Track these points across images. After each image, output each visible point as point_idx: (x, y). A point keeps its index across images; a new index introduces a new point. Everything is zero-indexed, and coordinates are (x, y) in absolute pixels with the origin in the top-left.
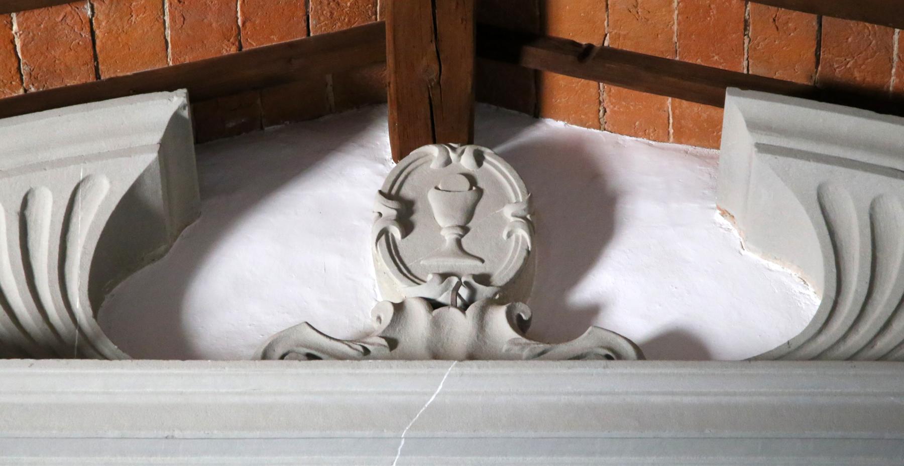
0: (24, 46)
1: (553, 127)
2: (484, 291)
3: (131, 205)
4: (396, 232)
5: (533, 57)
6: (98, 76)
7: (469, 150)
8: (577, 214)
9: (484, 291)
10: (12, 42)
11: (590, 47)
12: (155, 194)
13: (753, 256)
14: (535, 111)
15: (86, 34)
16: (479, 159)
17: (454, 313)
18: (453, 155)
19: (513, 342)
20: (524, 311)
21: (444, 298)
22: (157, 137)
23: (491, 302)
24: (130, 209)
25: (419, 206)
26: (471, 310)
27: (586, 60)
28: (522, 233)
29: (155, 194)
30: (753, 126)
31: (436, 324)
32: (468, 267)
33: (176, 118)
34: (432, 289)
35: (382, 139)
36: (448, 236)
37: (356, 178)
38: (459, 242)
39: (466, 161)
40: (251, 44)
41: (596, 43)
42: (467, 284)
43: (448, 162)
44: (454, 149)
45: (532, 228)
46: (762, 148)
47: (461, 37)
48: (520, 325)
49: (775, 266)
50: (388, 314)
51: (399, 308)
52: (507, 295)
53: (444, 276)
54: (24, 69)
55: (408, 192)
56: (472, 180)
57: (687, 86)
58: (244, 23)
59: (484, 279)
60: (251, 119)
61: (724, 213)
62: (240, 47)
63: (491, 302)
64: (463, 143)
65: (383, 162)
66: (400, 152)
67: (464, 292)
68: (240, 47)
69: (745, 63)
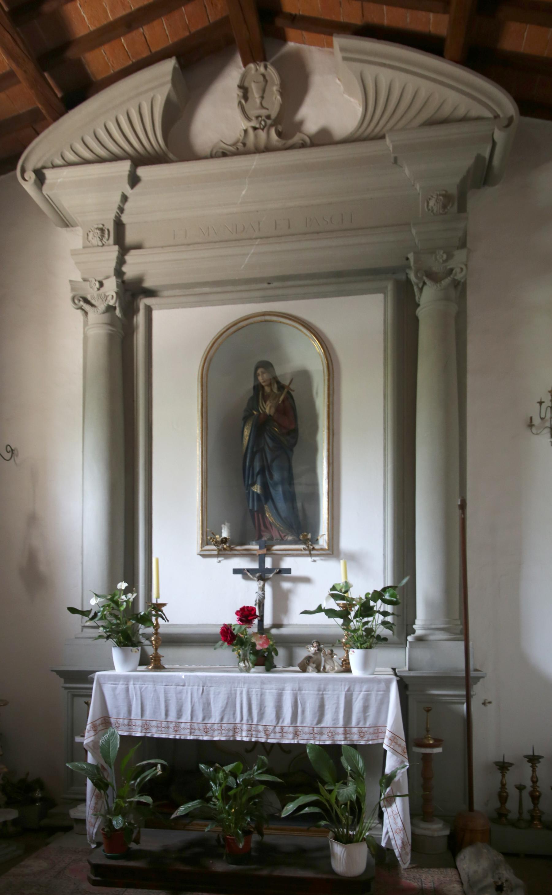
0: (127, 46)
1: (291, 45)
2: (269, 122)
3: (168, 103)
4: (243, 101)
5: (279, 22)
6: (151, 51)
7: (262, 64)
8: (296, 84)
9: (269, 122)
10: (123, 45)
11: (296, 15)
12: (174, 98)
13: (346, 96)
14: (284, 39)
15: (143, 38)
16: (266, 67)
17: (260, 131)
18: (258, 67)
19: (277, 141)
20: (280, 128)
21: (257, 126)
22: (169, 78)
23: (271, 126)
24: (169, 105)
25: (250, 89)
26: (265, 130)
27: (296, 20)
28: (279, 97)
29: (174, 98)
30: (342, 50)
31: (256, 136)
32: (264, 112)
33: (175, 69)
34: (254, 123)
35: (238, 59)
36: (258, 101)
37: (233, 74)
38: (261, 103)
39: (262, 69)
40: (193, 30)
41: (297, 13)
42: (264, 121)
43: (257, 70)
44: (258, 64)
45: (282, 94)
46: (345, 59)
47: (253, 19)
48: (279, 134)
49: (352, 100)
50: (243, 133)
51: (246, 131)
52: (276, 122)
53: (257, 117)
54: (130, 54)
55: (246, 84)
56: (264, 76)
57: (325, 28)
58: (189, 21)
59: (268, 117)
60: (197, 61)
61: (339, 79)
62: (190, 32)
63: (271, 126)
64: (261, 61)
65: (240, 68)
66: (245, 65)
67: (263, 123)
68: (190, 32)
69: (342, 18)
